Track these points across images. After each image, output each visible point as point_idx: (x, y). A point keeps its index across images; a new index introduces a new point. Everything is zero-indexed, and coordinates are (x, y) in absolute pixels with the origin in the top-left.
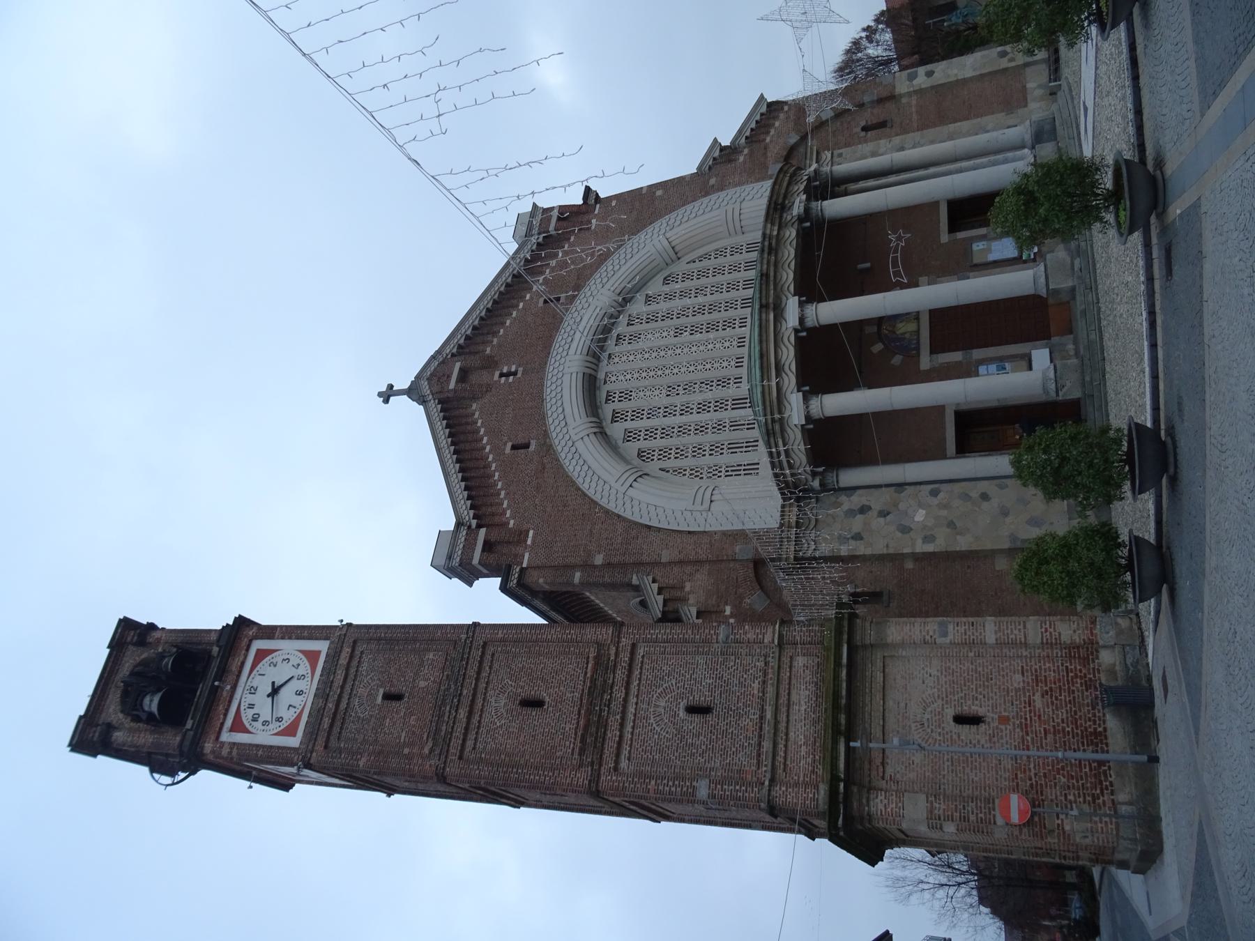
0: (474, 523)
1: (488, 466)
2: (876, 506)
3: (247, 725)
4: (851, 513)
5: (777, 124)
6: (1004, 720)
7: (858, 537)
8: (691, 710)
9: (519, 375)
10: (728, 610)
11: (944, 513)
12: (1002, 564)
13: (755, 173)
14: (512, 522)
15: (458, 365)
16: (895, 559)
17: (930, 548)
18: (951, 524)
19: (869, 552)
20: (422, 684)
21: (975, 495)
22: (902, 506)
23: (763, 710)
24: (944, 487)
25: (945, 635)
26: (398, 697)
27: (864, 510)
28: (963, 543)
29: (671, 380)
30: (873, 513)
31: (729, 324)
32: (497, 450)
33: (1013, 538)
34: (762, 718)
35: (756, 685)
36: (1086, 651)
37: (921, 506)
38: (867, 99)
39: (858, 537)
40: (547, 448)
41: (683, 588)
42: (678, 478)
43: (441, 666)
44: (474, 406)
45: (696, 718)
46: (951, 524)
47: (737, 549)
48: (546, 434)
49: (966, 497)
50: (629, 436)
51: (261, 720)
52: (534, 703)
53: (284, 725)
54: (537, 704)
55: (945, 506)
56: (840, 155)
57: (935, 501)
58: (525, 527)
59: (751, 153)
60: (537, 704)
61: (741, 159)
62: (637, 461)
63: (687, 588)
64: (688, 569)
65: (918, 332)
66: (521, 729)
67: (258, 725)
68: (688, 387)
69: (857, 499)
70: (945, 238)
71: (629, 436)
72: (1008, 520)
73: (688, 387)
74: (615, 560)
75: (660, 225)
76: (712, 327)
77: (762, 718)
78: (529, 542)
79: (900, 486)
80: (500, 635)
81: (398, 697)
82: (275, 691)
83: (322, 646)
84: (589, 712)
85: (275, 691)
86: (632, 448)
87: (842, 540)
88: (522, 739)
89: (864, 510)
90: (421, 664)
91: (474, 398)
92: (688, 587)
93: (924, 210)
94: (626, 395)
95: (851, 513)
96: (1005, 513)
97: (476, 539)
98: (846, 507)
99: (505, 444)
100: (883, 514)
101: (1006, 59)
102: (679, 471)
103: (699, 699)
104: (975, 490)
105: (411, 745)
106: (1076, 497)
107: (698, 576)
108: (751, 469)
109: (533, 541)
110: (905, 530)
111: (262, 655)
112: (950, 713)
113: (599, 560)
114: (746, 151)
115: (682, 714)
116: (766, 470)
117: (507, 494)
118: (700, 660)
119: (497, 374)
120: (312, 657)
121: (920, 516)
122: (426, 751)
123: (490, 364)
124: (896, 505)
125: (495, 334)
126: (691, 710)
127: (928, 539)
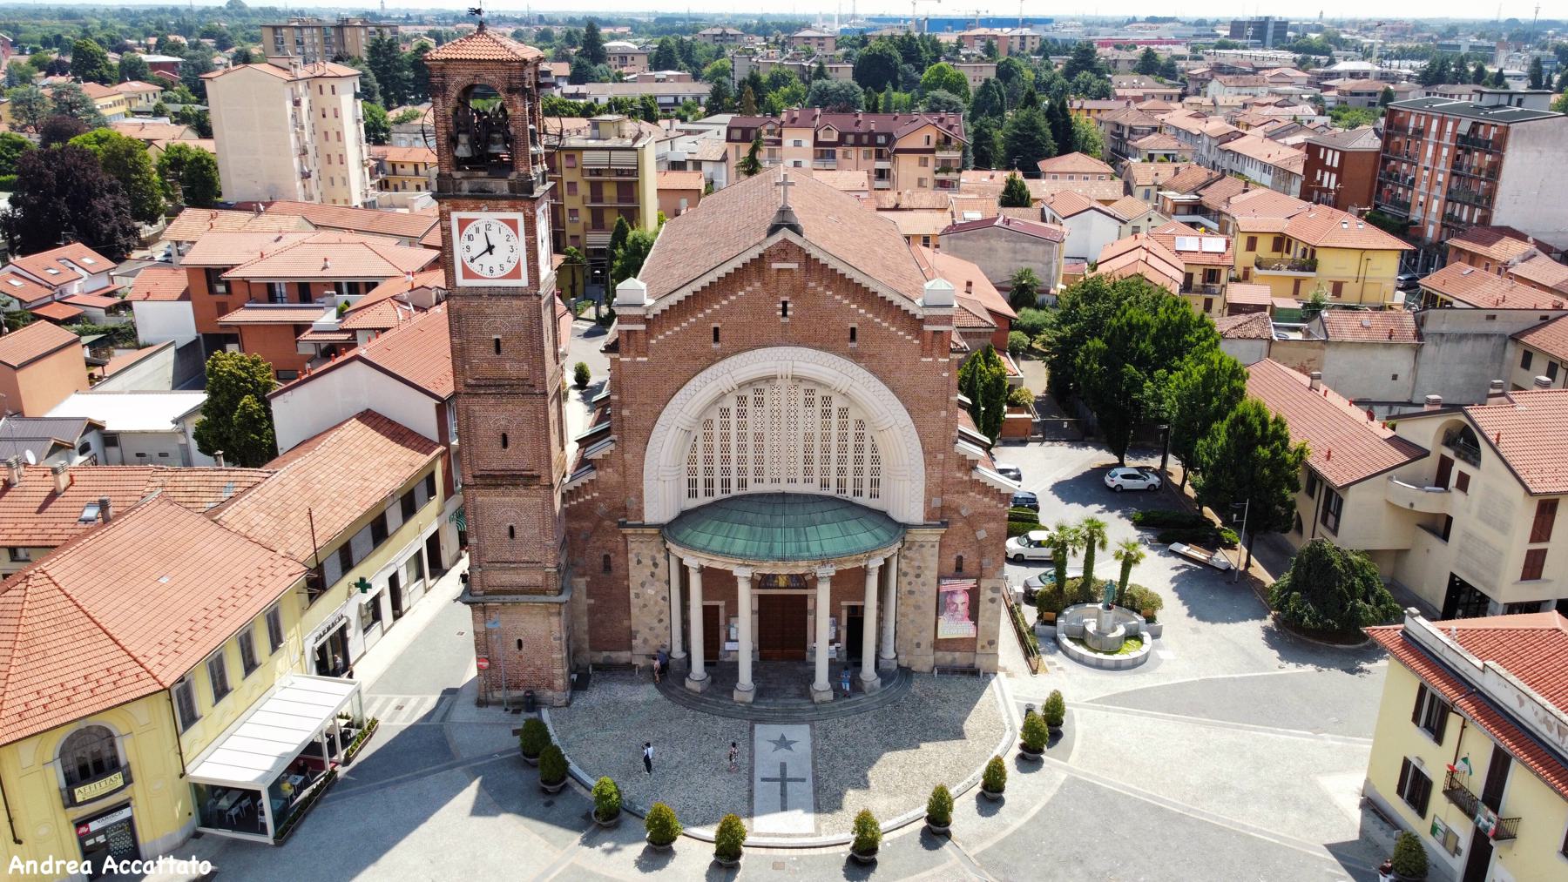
2: (657, 571)
4: (653, 558)
7: (639, 562)
8: (511, 528)
12: (626, 623)
13: (937, 488)
15: (794, 266)
17: (632, 596)
27: (655, 565)
28: (634, 611)
31: (807, 471)
32: (712, 318)
38: (985, 561)
39: (639, 562)
42: (685, 460)
44: (757, 284)
48: (724, 356)
49: (661, 612)
50: (725, 412)
54: (505, 445)
59: (961, 482)
60: (505, 445)
61: (959, 475)
65: (778, 588)
68: (759, 448)
71: (725, 412)
73: (759, 448)
75: (904, 417)
79: (668, 582)
81: (498, 351)
82: (490, 249)
83: (523, 282)
85: (490, 249)
86: (715, 416)
87: (637, 555)
89: (655, 565)
91: (764, 284)
94: (759, 402)
95: (653, 558)
96: (651, 629)
100: (653, 575)
102: (694, 447)
103: (517, 531)
104: (665, 617)
106: (1155, 340)
108: (693, 494)
110: (643, 585)
111: (512, 224)
113: (625, 413)
116: (692, 504)
120: (515, 274)
121: (651, 592)
125: (828, 287)
126: (511, 528)
127: (637, 596)
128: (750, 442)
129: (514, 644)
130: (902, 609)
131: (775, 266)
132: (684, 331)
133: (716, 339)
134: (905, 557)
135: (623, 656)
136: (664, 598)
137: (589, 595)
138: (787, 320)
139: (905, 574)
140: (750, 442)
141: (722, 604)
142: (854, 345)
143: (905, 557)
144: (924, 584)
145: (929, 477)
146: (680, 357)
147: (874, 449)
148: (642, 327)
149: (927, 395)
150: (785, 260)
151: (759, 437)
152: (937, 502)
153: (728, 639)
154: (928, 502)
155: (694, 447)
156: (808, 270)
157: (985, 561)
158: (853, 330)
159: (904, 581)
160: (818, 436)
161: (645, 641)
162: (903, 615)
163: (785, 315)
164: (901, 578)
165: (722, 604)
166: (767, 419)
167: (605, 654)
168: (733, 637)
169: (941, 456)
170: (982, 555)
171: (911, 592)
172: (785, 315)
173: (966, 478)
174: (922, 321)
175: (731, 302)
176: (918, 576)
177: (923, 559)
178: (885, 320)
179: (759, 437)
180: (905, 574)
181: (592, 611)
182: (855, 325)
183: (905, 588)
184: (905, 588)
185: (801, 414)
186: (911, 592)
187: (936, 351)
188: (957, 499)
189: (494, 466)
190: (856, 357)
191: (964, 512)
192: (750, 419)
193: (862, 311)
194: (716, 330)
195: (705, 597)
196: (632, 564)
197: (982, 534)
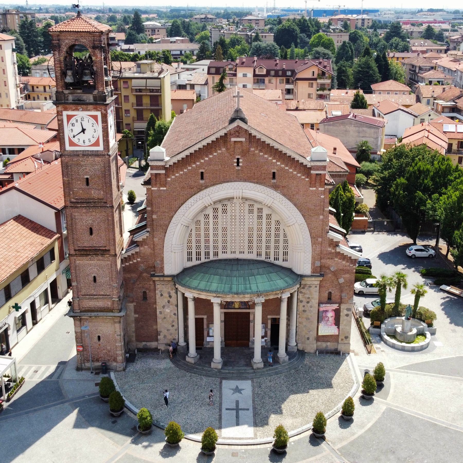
0: (168, 166)
1: (195, 163)
2: (171, 300)
3: (70, 122)
5: (344, 262)
6: (100, 345)
7: (162, 295)
9: (237, 168)
10: (139, 260)
11: (168, 316)
13: (318, 256)
14: (169, 179)
15: (243, 140)
16: (155, 303)
17: (158, 313)
18: (165, 318)
19: (157, 298)
20: (93, 192)
21: (173, 324)
22: (171, 306)
23: (96, 295)
24: (176, 317)
25: (117, 336)
26: (88, 184)
27: (170, 297)
28: (159, 321)
29: (229, 229)
30: (169, 299)
32: (199, 167)
33: (161, 332)
34: (94, 295)
35: (102, 293)
36: (115, 360)
37: (171, 311)
38: (343, 295)
39: (162, 295)
40: (200, 189)
41: (145, 245)
42: (186, 242)
43: (99, 197)
45: (92, 279)
46: (165, 318)
47: (158, 262)
48: (206, 187)
50: (207, 216)
51: (73, 128)
52: (91, 232)
53: (73, 139)
54: (91, 233)
55: (170, 316)
56: (316, 287)
57: (172, 314)
58: (167, 186)
59: (331, 253)
60: (91, 233)
61: (330, 249)
62: (195, 220)
63: (145, 247)
64: (152, 246)
66: (83, 229)
67: (71, 127)
68: (225, 235)
69: (173, 295)
70: (269, 317)
71: (207, 216)
72: (166, 331)
73: (225, 235)
74: (154, 223)
76: (250, 242)
77: (94, 295)
78: (161, 188)
79: (177, 306)
80: (110, 218)
81: (88, 184)
82: (83, 131)
83: (101, 148)
84: (90, 250)
85: (83, 131)
88: (81, 230)
89: (170, 297)
90: (99, 190)
91: (227, 149)
92: (146, 247)
93: (279, 313)
95: (169, 293)
96: (168, 330)
97: (160, 170)
98: (171, 292)
99: (204, 169)
100: (169, 302)
101: (343, 338)
102: (190, 235)
103: (97, 279)
105: (73, 193)
107: (150, 250)
109: (162, 190)
110: (164, 307)
111: (95, 118)
112: (100, 335)
113: (154, 217)
114: (333, 251)
115: (93, 275)
116: (190, 264)
117: (181, 174)
118: (108, 279)
119: (239, 157)
120: (97, 144)
121: (168, 311)
122: (72, 200)
123: (245, 153)
124: (172, 305)
125: (261, 151)
128: (220, 232)
129: (96, 338)
130: (300, 320)
131: (233, 139)
132: (185, 174)
133: (202, 178)
134: (301, 292)
135: (153, 344)
136: (175, 314)
137: (136, 312)
138: (239, 168)
139: (301, 302)
140: (220, 232)
141: (205, 317)
142: (274, 181)
143: (301, 292)
144: (311, 307)
145: (314, 250)
146: (183, 187)
147: (285, 236)
148: (163, 172)
149: (313, 207)
150: (238, 137)
151: (225, 229)
152: (318, 264)
153: (208, 336)
154: (313, 264)
155: (190, 235)
156: (250, 142)
157: (343, 295)
158: (274, 173)
159: (301, 305)
160: (255, 229)
161: (165, 336)
162: (300, 323)
163: (238, 165)
164: (299, 304)
165: (205, 317)
166: (229, 220)
167: (144, 343)
168: (211, 334)
169: (320, 240)
170: (342, 292)
171: (304, 311)
172: (238, 165)
173: (333, 251)
174: (310, 169)
175: (210, 159)
176: (308, 302)
177: (311, 293)
178: (290, 168)
179: (225, 229)
180: (301, 302)
181: (137, 321)
182: (275, 171)
183: (301, 308)
184: (301, 308)
185: (246, 217)
186: (304, 311)
187: (317, 184)
188: (328, 262)
189: (86, 244)
190: (275, 187)
191: (332, 269)
192: (220, 220)
193: (279, 163)
194: (202, 173)
195: (196, 313)
196: (158, 296)
197: (341, 281)
